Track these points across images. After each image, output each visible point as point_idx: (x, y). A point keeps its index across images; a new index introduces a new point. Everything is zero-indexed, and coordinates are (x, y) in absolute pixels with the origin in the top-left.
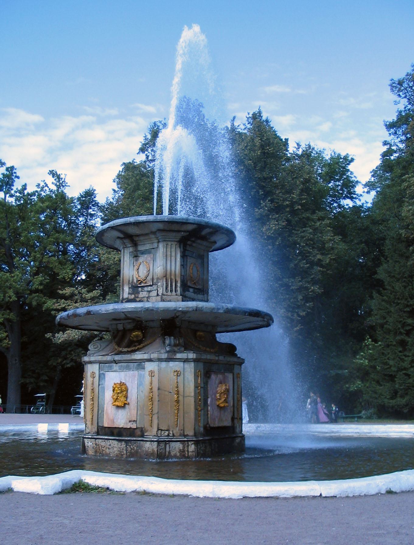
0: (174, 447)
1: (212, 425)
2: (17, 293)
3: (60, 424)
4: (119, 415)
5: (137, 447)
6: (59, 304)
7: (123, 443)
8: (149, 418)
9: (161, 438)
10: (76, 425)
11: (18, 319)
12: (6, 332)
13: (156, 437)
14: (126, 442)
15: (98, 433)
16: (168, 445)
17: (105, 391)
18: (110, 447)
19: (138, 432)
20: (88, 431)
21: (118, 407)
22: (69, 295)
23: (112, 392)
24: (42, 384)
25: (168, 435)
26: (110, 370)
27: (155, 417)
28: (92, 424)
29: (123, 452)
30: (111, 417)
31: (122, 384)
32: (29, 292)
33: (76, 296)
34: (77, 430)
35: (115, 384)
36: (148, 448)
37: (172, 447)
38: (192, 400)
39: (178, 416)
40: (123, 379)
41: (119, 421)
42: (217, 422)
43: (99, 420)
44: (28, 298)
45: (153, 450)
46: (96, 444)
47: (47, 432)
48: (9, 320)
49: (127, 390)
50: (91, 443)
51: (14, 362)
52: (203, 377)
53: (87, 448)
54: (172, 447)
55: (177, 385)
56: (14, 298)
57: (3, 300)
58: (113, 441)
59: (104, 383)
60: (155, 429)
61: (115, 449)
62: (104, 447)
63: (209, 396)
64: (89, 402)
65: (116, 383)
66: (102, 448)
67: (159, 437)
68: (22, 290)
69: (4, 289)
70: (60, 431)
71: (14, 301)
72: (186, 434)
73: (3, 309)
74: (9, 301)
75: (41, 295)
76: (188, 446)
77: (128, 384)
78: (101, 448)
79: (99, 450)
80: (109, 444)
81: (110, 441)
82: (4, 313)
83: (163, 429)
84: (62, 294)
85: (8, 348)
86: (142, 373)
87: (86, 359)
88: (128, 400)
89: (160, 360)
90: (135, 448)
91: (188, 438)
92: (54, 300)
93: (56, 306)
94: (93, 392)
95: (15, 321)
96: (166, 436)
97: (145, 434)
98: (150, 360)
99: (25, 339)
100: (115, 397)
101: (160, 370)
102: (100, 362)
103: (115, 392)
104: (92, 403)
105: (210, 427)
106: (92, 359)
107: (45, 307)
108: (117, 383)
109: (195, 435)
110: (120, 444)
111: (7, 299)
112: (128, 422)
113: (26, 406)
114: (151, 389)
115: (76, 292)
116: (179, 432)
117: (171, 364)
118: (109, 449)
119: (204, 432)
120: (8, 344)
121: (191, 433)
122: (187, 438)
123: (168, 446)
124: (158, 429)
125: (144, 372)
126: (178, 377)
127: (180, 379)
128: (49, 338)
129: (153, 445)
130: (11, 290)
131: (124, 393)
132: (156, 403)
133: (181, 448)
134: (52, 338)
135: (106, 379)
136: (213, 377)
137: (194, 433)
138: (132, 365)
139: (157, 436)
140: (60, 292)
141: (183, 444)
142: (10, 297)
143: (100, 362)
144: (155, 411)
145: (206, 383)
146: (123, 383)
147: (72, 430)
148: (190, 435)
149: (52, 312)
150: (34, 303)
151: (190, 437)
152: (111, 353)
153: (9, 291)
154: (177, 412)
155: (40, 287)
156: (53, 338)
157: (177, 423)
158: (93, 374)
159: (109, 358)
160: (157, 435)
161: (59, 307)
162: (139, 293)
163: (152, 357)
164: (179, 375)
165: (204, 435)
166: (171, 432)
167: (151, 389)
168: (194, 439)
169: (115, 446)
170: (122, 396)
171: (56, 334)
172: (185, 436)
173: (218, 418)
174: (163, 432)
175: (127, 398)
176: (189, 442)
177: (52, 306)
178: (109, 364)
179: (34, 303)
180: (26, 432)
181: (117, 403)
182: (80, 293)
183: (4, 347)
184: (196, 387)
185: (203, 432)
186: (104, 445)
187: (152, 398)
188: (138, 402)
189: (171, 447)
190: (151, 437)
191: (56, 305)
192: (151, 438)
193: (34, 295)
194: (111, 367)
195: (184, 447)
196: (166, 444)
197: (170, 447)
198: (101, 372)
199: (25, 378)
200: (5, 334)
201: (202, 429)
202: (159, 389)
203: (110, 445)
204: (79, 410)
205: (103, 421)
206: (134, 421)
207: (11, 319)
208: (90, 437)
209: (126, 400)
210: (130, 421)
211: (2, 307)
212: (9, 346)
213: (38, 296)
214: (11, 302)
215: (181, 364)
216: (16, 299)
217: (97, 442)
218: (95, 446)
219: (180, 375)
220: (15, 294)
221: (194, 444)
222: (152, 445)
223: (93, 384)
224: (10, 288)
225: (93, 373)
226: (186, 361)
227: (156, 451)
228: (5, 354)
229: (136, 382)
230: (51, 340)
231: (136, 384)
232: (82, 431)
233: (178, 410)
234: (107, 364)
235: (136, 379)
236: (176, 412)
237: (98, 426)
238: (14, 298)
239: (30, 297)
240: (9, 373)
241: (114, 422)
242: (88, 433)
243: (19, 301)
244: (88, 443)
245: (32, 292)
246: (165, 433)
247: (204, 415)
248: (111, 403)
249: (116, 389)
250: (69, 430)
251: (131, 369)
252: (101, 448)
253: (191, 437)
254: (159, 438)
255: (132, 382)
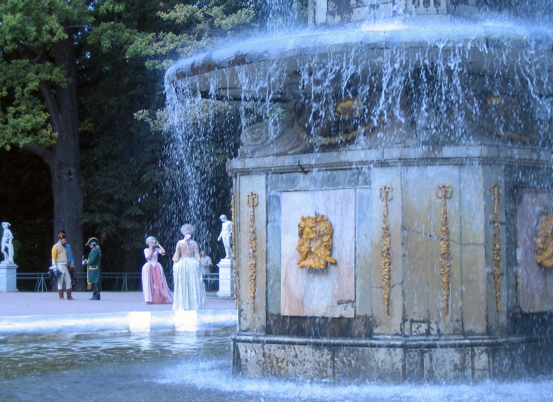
0: (442, 359)
1: (526, 310)
2: (66, 23)
3: (130, 313)
4: (314, 289)
5: (358, 360)
6: (161, 43)
7: (326, 351)
8: (379, 294)
9: (410, 338)
10: (214, 313)
11: (71, 80)
12: (45, 111)
13: (399, 337)
14: (334, 348)
15: (268, 331)
16: (427, 355)
17: (282, 237)
18: (296, 361)
19: (358, 327)
20: (245, 325)
21: (312, 271)
22: (183, 22)
23: (298, 237)
24: (129, 225)
25: (428, 333)
26: (293, 188)
27: (397, 291)
28: (255, 310)
29: (326, 372)
30: (297, 292)
31: (319, 219)
32: (93, 19)
33: (199, 22)
34: (215, 326)
35: (304, 219)
36: (382, 362)
37: (437, 359)
38: (481, 252)
39: (449, 289)
40: (322, 207)
41: (315, 301)
42: (537, 302)
43: (269, 302)
44: (92, 32)
45: (393, 365)
46: (264, 355)
47: (148, 330)
48: (50, 85)
49: (331, 233)
50: (253, 353)
51: (66, 178)
52: (502, 199)
53: (243, 362)
54: (437, 359)
55: (446, 218)
56: (61, 34)
57: (36, 39)
58: (302, 347)
59: (280, 216)
60: (397, 320)
61: (308, 365)
62: (282, 362)
63: (519, 243)
64: (246, 262)
65: (305, 216)
66: (277, 362)
67: (406, 336)
68: (78, 16)
69: (37, 14)
70: (177, 327)
71: (61, 41)
72: (467, 329)
73: (36, 59)
74: (50, 41)
75: (121, 25)
76: (472, 357)
77: (332, 219)
78: (275, 362)
79: (272, 367)
80: (293, 354)
81: (296, 346)
82: (38, 68)
83: (416, 319)
84: (169, 20)
85: (51, 148)
86: (366, 192)
87: (235, 164)
88: (335, 255)
89: (406, 162)
90: (353, 362)
91: (473, 339)
92: (150, 36)
93: (156, 48)
94: (255, 239)
95: (64, 85)
96: (423, 335)
97: (376, 331)
98: (383, 164)
99: (87, 126)
100: (304, 249)
101: (404, 186)
102: (267, 171)
103: (304, 236)
104: (253, 262)
105: (521, 313)
106: (250, 163)
107: (130, 50)
108: (309, 218)
109: (489, 332)
110: (317, 353)
111: (46, 38)
112: (335, 303)
113: (121, 276)
114: (387, 228)
115: (200, 15)
116: (452, 324)
117: (431, 171)
118: (293, 365)
119: (507, 324)
120: (51, 138)
121: (480, 328)
122: (469, 339)
123: (427, 356)
124: (404, 320)
125: (369, 190)
126: (448, 201)
127: (452, 205)
128: (142, 120)
129: (393, 355)
130: (54, 17)
131: (326, 239)
132: (398, 262)
133: (458, 362)
134: (148, 120)
135: (283, 208)
136: (527, 198)
137: (485, 327)
138: (341, 175)
139: (403, 334)
140: (164, 16)
141: (460, 352)
142: (52, 32)
143: (267, 171)
144: (397, 278)
145: (512, 215)
146: (323, 216)
147: (204, 325)
148: (477, 332)
149: (146, 64)
150: (106, 44)
151: (476, 337)
152: (293, 149)
153: (48, 18)
154: (447, 279)
155: (117, 7)
156: (152, 120)
157: (447, 306)
158: (253, 199)
159: (288, 161)
160: (403, 333)
161: (163, 51)
162: (353, 12)
163: (386, 157)
164: (448, 195)
165: (511, 332)
166: (434, 326)
167: (387, 228)
168: (486, 341)
169: (307, 357)
170: (320, 246)
171: (157, 111)
172: (465, 334)
173: (541, 293)
174: (415, 326)
175: (331, 250)
176: (476, 348)
177: (146, 49)
178: (288, 175)
179: (106, 44)
180: (103, 330)
181: (309, 262)
182: (207, 17)
183: (41, 146)
184: (490, 223)
185: (505, 325)
186: (283, 357)
187: (388, 250)
188: (358, 259)
189: (434, 358)
190: (389, 337)
191: (156, 45)
192: (388, 339)
193: (104, 25)
194: (294, 180)
195: (464, 359)
196: (423, 353)
197: (431, 360)
198: (273, 193)
199: (92, 212)
200: (42, 118)
201: (503, 319)
202: (404, 228)
203: (296, 356)
204: (18, 273)
205: (280, 302)
206: (349, 302)
207: (54, 82)
208: (250, 338)
209: (330, 255)
210: (339, 303)
211: (35, 56)
212: (54, 142)
213: (113, 28)
214: (53, 44)
215: (453, 171)
216: (66, 37)
217: (266, 351)
218: (263, 359)
219: (451, 194)
220: (61, 24)
221: (486, 351)
222: (390, 354)
223: (253, 220)
224: (50, 12)
225: (254, 196)
226: (459, 163)
227: (400, 368)
228: (46, 161)
229: (352, 214)
230: (148, 124)
231: (352, 220)
232: (226, 329)
233: (449, 276)
234: (284, 176)
235: (351, 206)
236: (444, 280)
237: (268, 315)
238: (61, 34)
239: (96, 30)
240: (56, 204)
241: (302, 304)
242: (245, 331)
243: (71, 38)
244: (246, 351)
245: (99, 18)
246: (420, 329)
247: (508, 286)
248: (295, 262)
249: (307, 229)
250: (198, 326)
251: (339, 185)
252: (275, 362)
253: (479, 337)
254: (407, 339)
255: (342, 215)
